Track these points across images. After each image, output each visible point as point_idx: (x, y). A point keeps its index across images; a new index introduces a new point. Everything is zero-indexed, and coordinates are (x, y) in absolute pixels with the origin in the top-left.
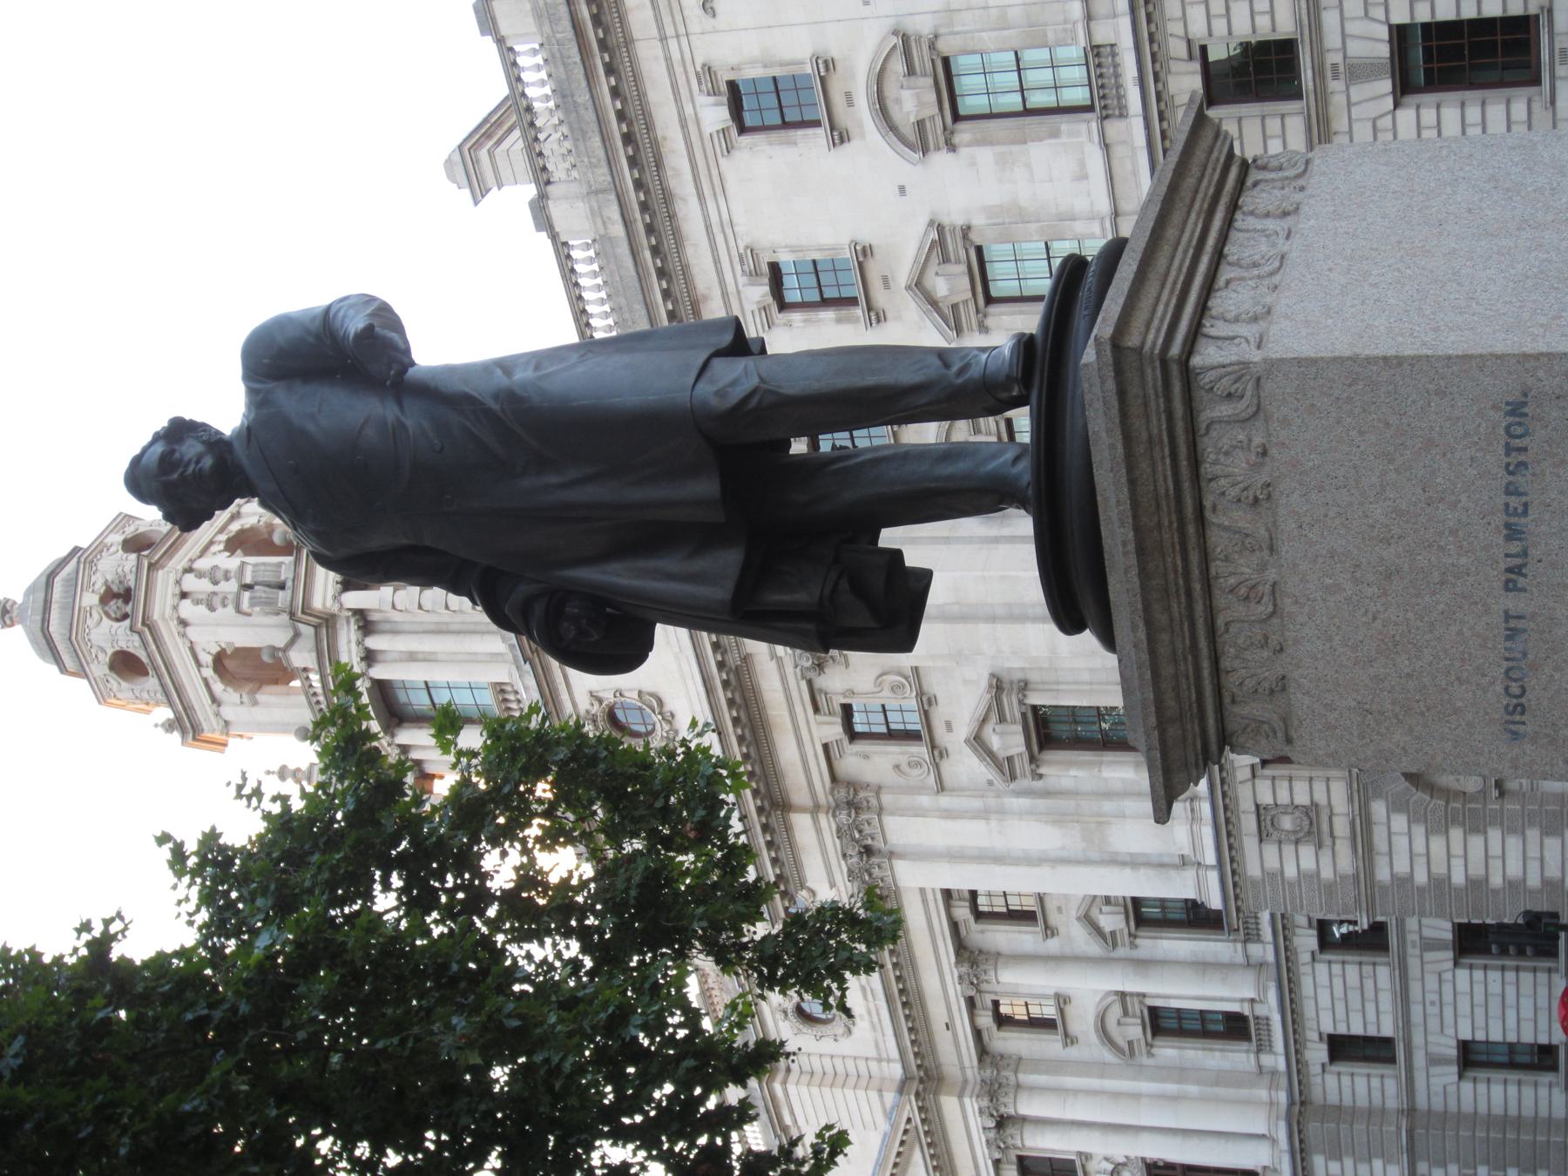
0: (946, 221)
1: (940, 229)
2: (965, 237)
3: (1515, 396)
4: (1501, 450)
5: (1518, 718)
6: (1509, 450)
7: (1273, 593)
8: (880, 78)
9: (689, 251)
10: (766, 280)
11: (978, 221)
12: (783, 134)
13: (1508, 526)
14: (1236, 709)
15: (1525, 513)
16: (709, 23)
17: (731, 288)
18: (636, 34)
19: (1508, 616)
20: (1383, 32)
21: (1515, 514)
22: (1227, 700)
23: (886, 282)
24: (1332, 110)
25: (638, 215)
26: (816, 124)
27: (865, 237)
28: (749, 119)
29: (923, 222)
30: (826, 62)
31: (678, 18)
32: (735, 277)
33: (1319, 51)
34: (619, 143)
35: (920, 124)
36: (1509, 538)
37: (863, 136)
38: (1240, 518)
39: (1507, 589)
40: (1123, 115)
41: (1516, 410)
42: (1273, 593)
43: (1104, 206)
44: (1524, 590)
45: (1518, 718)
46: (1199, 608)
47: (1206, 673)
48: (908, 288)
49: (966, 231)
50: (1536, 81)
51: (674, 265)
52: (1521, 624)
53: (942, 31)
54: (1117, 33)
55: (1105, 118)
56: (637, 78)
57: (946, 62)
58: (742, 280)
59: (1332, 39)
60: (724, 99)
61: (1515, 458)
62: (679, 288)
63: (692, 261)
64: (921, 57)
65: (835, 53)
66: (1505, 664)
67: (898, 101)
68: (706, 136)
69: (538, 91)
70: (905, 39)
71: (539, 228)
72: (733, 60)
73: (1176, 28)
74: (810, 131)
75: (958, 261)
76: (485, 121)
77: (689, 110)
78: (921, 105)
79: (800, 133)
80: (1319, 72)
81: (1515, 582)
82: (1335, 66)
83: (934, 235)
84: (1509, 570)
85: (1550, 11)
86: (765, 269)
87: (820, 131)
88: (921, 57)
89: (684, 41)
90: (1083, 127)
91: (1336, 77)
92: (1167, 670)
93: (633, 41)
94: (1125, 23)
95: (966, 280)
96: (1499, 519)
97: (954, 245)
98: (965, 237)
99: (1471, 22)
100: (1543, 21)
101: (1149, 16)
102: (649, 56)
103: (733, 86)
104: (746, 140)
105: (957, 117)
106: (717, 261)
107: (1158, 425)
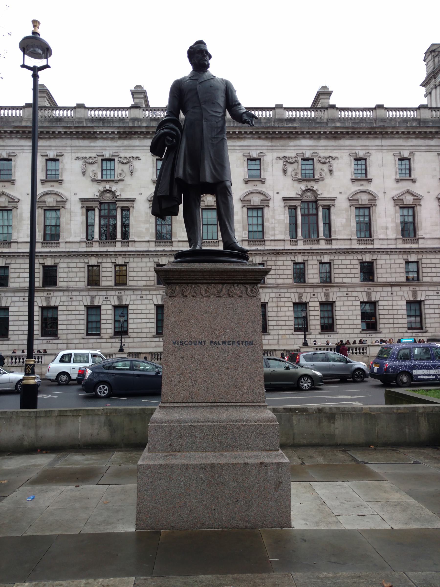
0: (19, 203)
1: (18, 202)
2: (15, 207)
3: (254, 343)
4: (242, 340)
5: (179, 343)
6: (242, 342)
7: (207, 296)
8: (57, 194)
9: (17, 140)
10: (7, 157)
11: (19, 211)
12: (45, 169)
13: (225, 341)
14: (178, 286)
15: (228, 345)
16: (74, 158)
17: (6, 148)
18: (73, 141)
19: (204, 341)
20: (57, 305)
21: (228, 343)
22: (180, 285)
23: (5, 186)
24: (40, 293)
25: (28, 130)
26: (46, 177)
27: (17, 183)
28: (49, 163)
29: (20, 198)
30: (61, 183)
31: (76, 151)
32: (9, 150)
33: (53, 291)
34: (47, 130)
35: (45, 201)
36: (223, 342)
37: (43, 188)
38: (224, 291)
39: (211, 341)
40: (42, 247)
41: (251, 343)
42: (207, 296)
43: (20, 240)
44: (211, 344)
45: (179, 343)
46: (205, 281)
47: (183, 281)
48: (3, 192)
49: (17, 208)
50: (42, 336)
51: (13, 136)
52: (203, 343)
53: (66, 210)
54: (62, 248)
55: (42, 243)
56: (63, 138)
57: (59, 210)
58: (8, 152)
59: (56, 294)
60: (55, 157)
61: (240, 343)
62: (7, 135)
63: (14, 140)
64: (60, 204)
65: (63, 185)
66: (193, 341)
67: (51, 197)
68: (46, 151)
69: (57, 113)
70: (65, 201)
71: (26, 104)
72: (64, 161)
73: (62, 261)
74: (45, 176)
75: (8, 204)
76: (53, 98)
77: (53, 148)
78: (49, 202)
79: (45, 173)
80: (49, 290)
81: (213, 343)
82: (50, 294)
83: (16, 200)
84: (215, 342)
85: (58, 339)
86: (10, 158)
87: (45, 178)
88: (60, 204)
89: (70, 151)
90: (40, 238)
91: (47, 294)
92: (192, 274)
93: (71, 139)
94: (64, 250)
95: (4, 206)
96: (227, 340)
97: (13, 204)
98: (15, 207)
99: (57, 323)
100: (56, 338)
101: (66, 255)
102: (68, 142)
103: (58, 160)
104: (44, 160)
105: (45, 210)
106: (13, 146)
107: (248, 277)
